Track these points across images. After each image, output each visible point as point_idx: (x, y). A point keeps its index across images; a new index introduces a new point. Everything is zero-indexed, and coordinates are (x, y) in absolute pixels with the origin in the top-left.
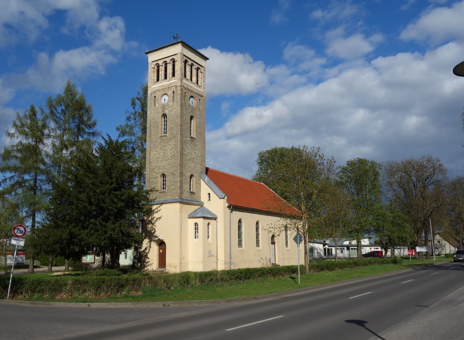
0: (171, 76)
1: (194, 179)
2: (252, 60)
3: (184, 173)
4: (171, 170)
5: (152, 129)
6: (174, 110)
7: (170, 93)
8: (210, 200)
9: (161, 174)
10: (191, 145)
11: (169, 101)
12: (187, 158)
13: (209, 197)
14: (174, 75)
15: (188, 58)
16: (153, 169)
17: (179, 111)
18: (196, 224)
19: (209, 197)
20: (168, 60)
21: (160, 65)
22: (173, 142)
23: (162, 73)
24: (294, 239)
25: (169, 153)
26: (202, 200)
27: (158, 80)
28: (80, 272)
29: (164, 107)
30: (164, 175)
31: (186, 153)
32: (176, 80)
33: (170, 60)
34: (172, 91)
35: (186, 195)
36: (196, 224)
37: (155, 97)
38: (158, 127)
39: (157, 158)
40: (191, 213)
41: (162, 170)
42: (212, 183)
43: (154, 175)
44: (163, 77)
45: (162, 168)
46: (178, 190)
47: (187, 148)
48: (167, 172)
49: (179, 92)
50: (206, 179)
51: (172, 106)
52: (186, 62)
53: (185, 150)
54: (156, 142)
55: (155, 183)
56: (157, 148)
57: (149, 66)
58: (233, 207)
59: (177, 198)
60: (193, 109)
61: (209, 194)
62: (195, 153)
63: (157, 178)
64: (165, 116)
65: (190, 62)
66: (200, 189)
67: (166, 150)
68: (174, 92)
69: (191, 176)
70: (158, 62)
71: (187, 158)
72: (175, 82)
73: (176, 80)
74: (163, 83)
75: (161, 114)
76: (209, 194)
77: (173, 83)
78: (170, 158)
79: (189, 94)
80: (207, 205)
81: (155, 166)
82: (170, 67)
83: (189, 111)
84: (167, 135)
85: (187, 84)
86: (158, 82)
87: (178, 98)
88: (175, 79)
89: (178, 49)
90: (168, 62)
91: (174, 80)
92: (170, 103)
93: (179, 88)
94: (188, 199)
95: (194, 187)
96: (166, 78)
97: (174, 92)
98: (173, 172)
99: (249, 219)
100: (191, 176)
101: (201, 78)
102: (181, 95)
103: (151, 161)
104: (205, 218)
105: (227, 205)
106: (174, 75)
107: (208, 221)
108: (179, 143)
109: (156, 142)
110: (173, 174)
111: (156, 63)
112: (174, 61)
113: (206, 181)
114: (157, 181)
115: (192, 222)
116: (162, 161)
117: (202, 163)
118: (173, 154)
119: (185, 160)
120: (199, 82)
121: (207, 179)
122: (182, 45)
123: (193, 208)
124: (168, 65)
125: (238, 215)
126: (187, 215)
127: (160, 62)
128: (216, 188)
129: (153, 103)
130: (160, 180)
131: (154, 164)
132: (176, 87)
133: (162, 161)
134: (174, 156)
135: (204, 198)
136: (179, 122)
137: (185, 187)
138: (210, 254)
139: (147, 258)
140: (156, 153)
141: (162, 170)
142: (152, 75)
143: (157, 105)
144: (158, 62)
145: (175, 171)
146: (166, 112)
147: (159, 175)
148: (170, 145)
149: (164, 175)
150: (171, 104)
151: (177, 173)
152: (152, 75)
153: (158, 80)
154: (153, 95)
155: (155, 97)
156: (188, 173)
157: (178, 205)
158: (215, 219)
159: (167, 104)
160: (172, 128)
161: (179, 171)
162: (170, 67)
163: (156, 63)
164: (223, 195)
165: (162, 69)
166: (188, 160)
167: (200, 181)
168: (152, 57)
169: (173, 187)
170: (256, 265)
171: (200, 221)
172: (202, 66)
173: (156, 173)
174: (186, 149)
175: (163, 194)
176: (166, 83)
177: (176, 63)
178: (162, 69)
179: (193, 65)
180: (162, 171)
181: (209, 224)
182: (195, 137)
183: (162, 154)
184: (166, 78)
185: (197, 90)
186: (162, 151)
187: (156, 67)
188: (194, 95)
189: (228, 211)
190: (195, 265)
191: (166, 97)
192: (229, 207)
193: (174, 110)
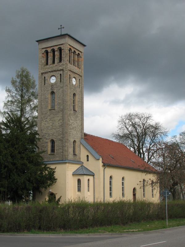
9: (50, 139)
24: (78, 191)
26: (81, 160)
28: (134, 230)
29: (52, 85)
33: (57, 48)
38: (47, 102)
39: (47, 127)
40: (75, 171)
41: (51, 137)
43: (45, 140)
48: (56, 139)
55: (46, 147)
58: (105, 165)
61: (88, 156)
62: (77, 123)
63: (47, 142)
64: (53, 93)
70: (54, 48)
71: (71, 127)
75: (50, 91)
76: (88, 156)
78: (58, 127)
80: (86, 164)
82: (57, 53)
103: (42, 129)
114: (47, 145)
116: (51, 129)
118: (60, 124)
123: (77, 166)
124: (49, 54)
125: (110, 172)
128: (93, 152)
130: (49, 145)
131: (44, 132)
133: (51, 129)
134: (61, 126)
135: (83, 159)
137: (70, 151)
140: (46, 123)
141: (51, 137)
144: (54, 48)
149: (53, 142)
153: (47, 64)
162: (57, 53)
163: (52, 48)
165: (50, 55)
166: (73, 129)
172: (81, 52)
173: (46, 139)
174: (70, 120)
175: (52, 156)
178: (50, 55)
184: (54, 62)
186: (51, 121)
187: (45, 54)
191: (54, 78)
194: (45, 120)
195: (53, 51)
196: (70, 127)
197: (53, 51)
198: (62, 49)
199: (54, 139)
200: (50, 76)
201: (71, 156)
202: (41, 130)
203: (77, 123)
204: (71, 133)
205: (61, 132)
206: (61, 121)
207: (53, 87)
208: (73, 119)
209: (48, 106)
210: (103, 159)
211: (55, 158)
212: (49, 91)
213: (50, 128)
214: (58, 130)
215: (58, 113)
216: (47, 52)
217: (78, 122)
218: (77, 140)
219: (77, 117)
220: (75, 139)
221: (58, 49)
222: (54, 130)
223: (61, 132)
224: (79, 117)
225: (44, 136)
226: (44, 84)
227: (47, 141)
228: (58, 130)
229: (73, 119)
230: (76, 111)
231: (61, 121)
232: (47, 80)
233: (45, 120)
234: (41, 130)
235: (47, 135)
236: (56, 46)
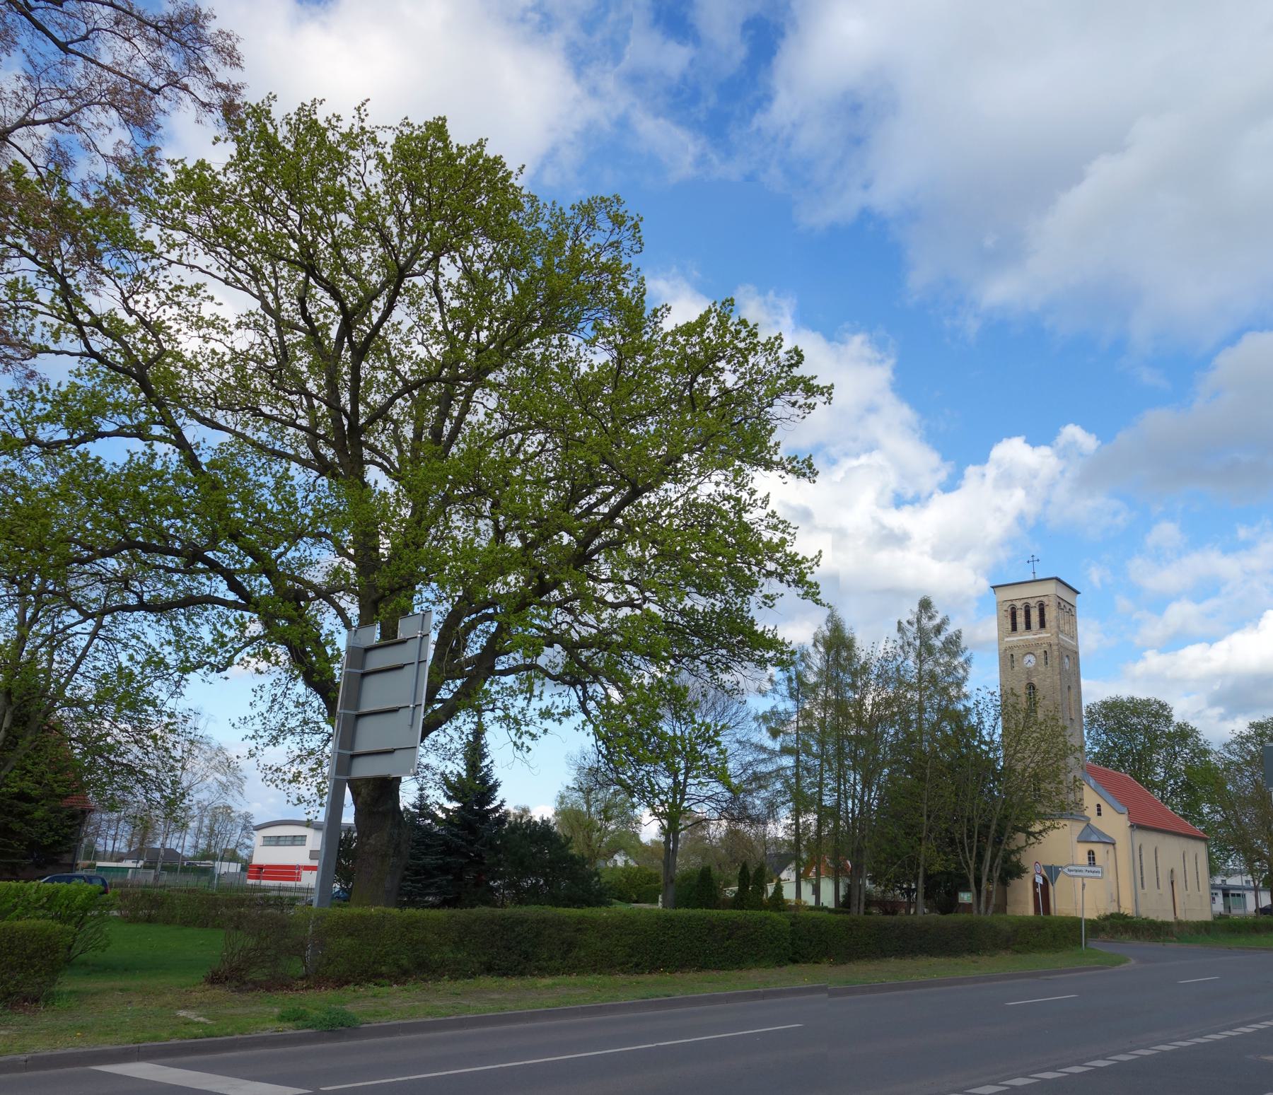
2: (922, 460)
7: (1039, 652)
8: (1099, 814)
11: (1037, 664)
14: (1042, 624)
18: (1091, 853)
23: (1021, 620)
27: (1014, 628)
29: (1029, 672)
36: (1091, 853)
42: (1103, 791)
49: (1056, 653)
58: (1136, 826)
64: (1031, 687)
75: (1024, 683)
80: (1095, 821)
82: (1035, 615)
86: (1014, 634)
96: (1028, 626)
106: (1042, 624)
125: (1141, 837)
126: (1075, 838)
128: (1110, 798)
135: (1091, 812)
139: (563, 846)
144: (1029, 601)
146: (1035, 681)
150: (1042, 669)
153: (1014, 628)
162: (1035, 615)
164: (1125, 810)
176: (1029, 636)
177: (1046, 610)
189: (1129, 830)
191: (1031, 658)
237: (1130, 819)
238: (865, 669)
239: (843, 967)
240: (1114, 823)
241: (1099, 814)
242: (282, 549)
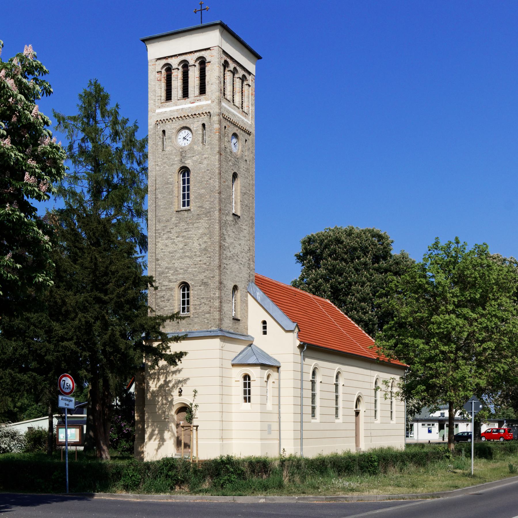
0: (197, 91)
1: (238, 294)
3: (225, 282)
4: (201, 277)
5: (159, 196)
6: (205, 162)
7: (196, 125)
8: (265, 333)
9: (179, 282)
10: (234, 230)
11: (193, 142)
12: (229, 254)
13: (265, 328)
14: (203, 90)
15: (232, 58)
16: (163, 273)
17: (217, 163)
18: (247, 377)
19: (265, 328)
20: (191, 59)
21: (174, 67)
22: (203, 223)
25: (196, 244)
26: (249, 333)
27: (169, 97)
29: (183, 153)
30: (185, 286)
31: (226, 245)
32: (209, 102)
34: (200, 123)
35: (227, 324)
36: (247, 377)
37: (164, 132)
38: (171, 192)
41: (181, 276)
43: (166, 283)
44: (180, 93)
45: (181, 271)
46: (217, 315)
47: (229, 236)
48: (192, 280)
49: (216, 126)
50: (258, 294)
51: (200, 153)
52: (226, 65)
53: (225, 239)
54: (168, 221)
56: (170, 232)
57: (150, 68)
58: (309, 348)
59: (213, 328)
60: (237, 159)
61: (264, 322)
62: (240, 245)
63: (171, 289)
64: (185, 171)
65: (232, 65)
66: (247, 312)
67: (189, 238)
68: (204, 125)
69: (235, 288)
70: (169, 61)
71: (229, 254)
72: (208, 105)
73: (209, 102)
74: (178, 106)
75: (177, 167)
76: (264, 322)
77: (202, 106)
78: (198, 253)
79: (230, 129)
80: (260, 342)
81: (166, 268)
82: (194, 74)
83: (230, 163)
84: (192, 206)
85: (228, 111)
86: (203, 97)
87: (213, 137)
88: (207, 100)
89: (212, 39)
90: (191, 62)
91: (205, 103)
92: (195, 147)
93: (215, 118)
94: (230, 332)
95: (238, 309)
96: (185, 94)
97: (204, 125)
98: (205, 280)
99: (328, 369)
100: (235, 288)
101: (249, 97)
102: (220, 133)
103: (159, 257)
104: (263, 366)
105: (298, 343)
106: (203, 90)
107: (266, 372)
108: (217, 227)
109: (168, 221)
110: (205, 284)
111: (164, 62)
112: (203, 63)
113: (259, 298)
114: (171, 295)
115: (239, 373)
116: (181, 258)
117: (249, 264)
118: (203, 246)
119: (226, 259)
120: (245, 105)
121: (259, 294)
122: (222, 34)
123: (239, 348)
124: (191, 69)
127: (175, 62)
129: (160, 143)
130: (178, 294)
131: (164, 264)
132: (209, 114)
133: (181, 258)
134: (205, 249)
135: (254, 329)
136: (217, 184)
138: (270, 428)
141: (181, 276)
142: (156, 86)
143: (168, 149)
144: (169, 61)
145: (209, 278)
146: (189, 164)
147: (175, 285)
148: (198, 228)
149: (185, 286)
150: (198, 148)
151: (214, 284)
152: (156, 86)
153: (169, 97)
154: (160, 128)
155: (164, 132)
156: (230, 282)
157: (217, 340)
158: (278, 368)
159: (191, 148)
160: (201, 196)
161: (217, 278)
162: (194, 74)
163: (164, 62)
164: (292, 326)
166: (231, 258)
167: (247, 296)
168: (156, 51)
169: (206, 308)
170: (76, 501)
171: (255, 373)
173: (170, 281)
174: (227, 237)
177: (208, 68)
179: (246, 78)
180: (181, 278)
181: (268, 377)
182: (239, 214)
183: (181, 246)
184: (185, 94)
185: (243, 121)
186: (180, 239)
187: (163, 71)
188: (239, 132)
190: (244, 447)
192: (301, 347)
193: (205, 162)
194: (165, 237)
195: (185, 65)
196: (225, 252)
197: (185, 65)
198: (208, 60)
199: (189, 282)
200: (178, 128)
201: (229, 322)
202: (157, 260)
203: (240, 245)
204: (227, 267)
205: (205, 264)
206: (205, 239)
207: (184, 157)
208: (232, 234)
209: (172, 203)
210: (299, 331)
211: (191, 326)
212: (175, 166)
213: (178, 255)
214: (199, 259)
215: (197, 219)
216: (169, 69)
217: (243, 242)
218: (240, 286)
219: (240, 230)
220: (236, 282)
221: (179, 65)
222: (188, 260)
223: (205, 264)
224: (245, 232)
225: (163, 273)
226: (161, 148)
227: (171, 285)
228: (199, 259)
229: (232, 234)
230: (239, 217)
231: (205, 239)
232: (169, 138)
233: (165, 237)
234: (157, 260)
235: (171, 272)
236: (191, 52)
237: (299, 336)
238: (143, 151)
239: (38, 506)
240: (281, 343)
241: (265, 333)
242: (73, 448)
